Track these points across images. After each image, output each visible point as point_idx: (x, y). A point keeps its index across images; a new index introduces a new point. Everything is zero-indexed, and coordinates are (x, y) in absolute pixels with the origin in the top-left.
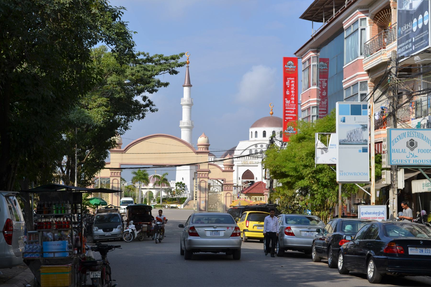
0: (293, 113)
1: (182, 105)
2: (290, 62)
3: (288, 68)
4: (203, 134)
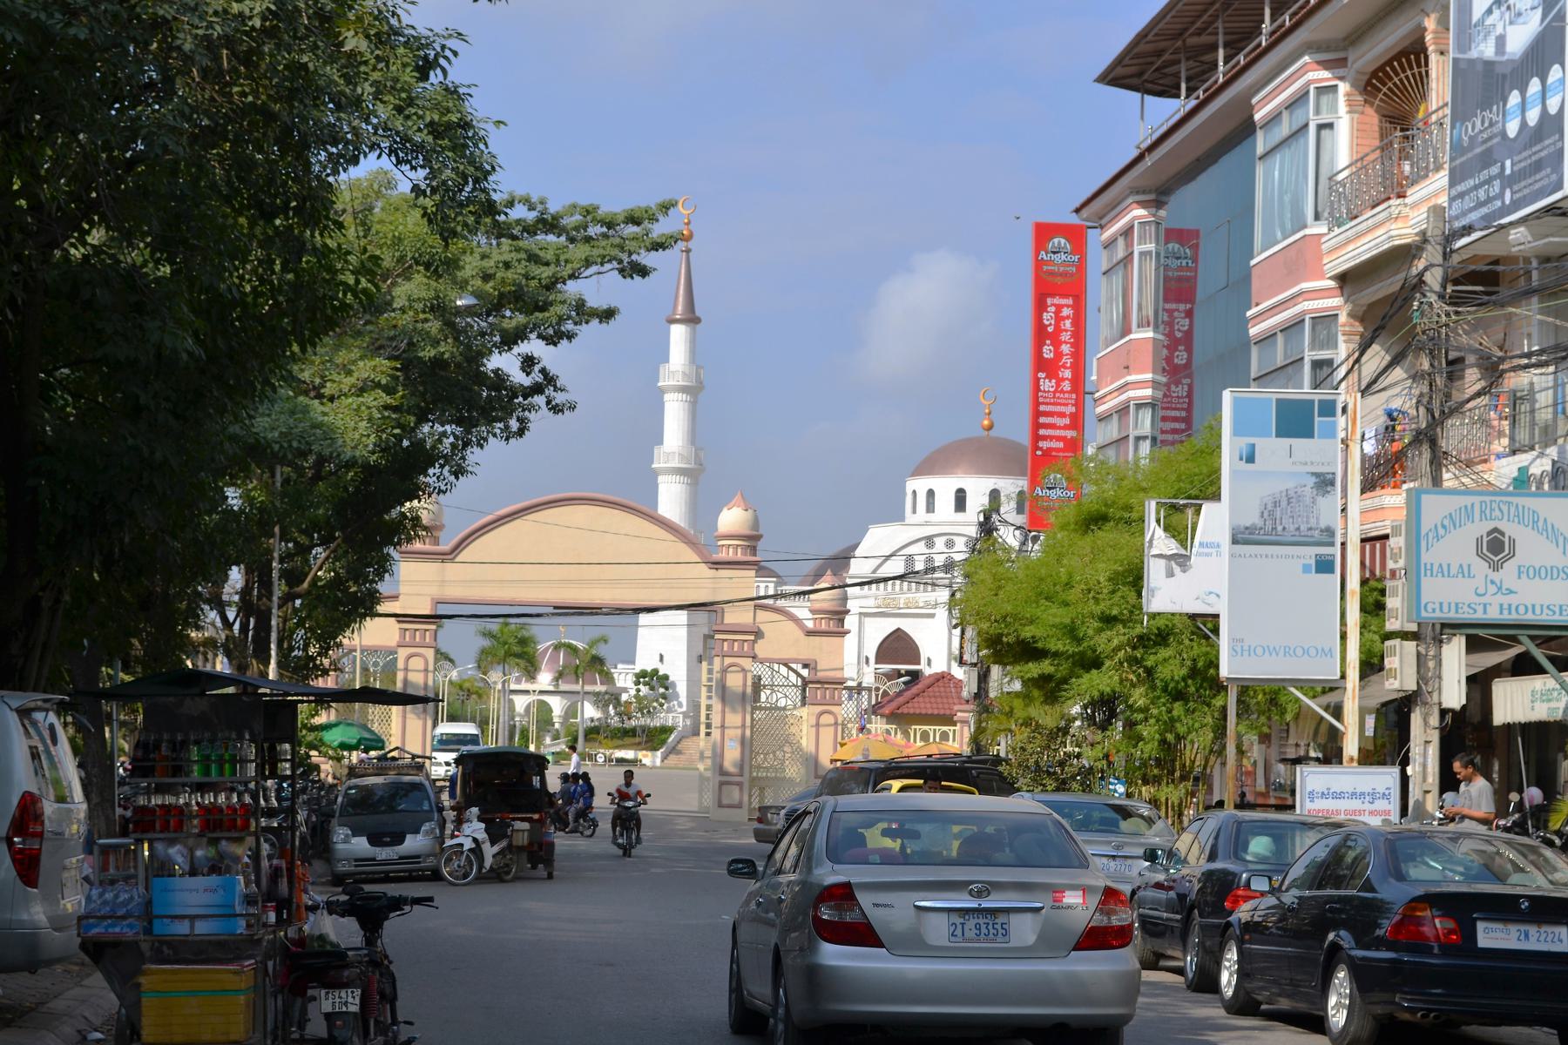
0: (1065, 427)
1: (662, 391)
3: (1050, 262)
4: (738, 496)
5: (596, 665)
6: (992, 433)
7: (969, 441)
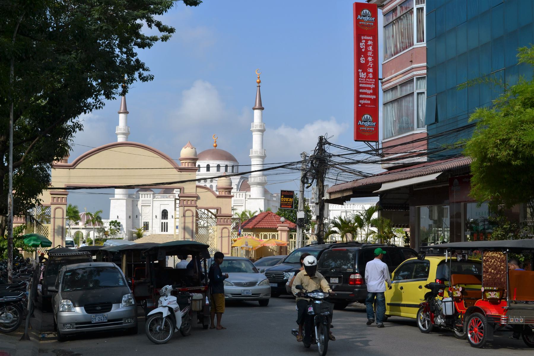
0: (371, 94)
1: (117, 134)
2: (366, 11)
3: (362, 21)
4: (188, 143)
5: (97, 219)
6: (216, 148)
7: (210, 150)
